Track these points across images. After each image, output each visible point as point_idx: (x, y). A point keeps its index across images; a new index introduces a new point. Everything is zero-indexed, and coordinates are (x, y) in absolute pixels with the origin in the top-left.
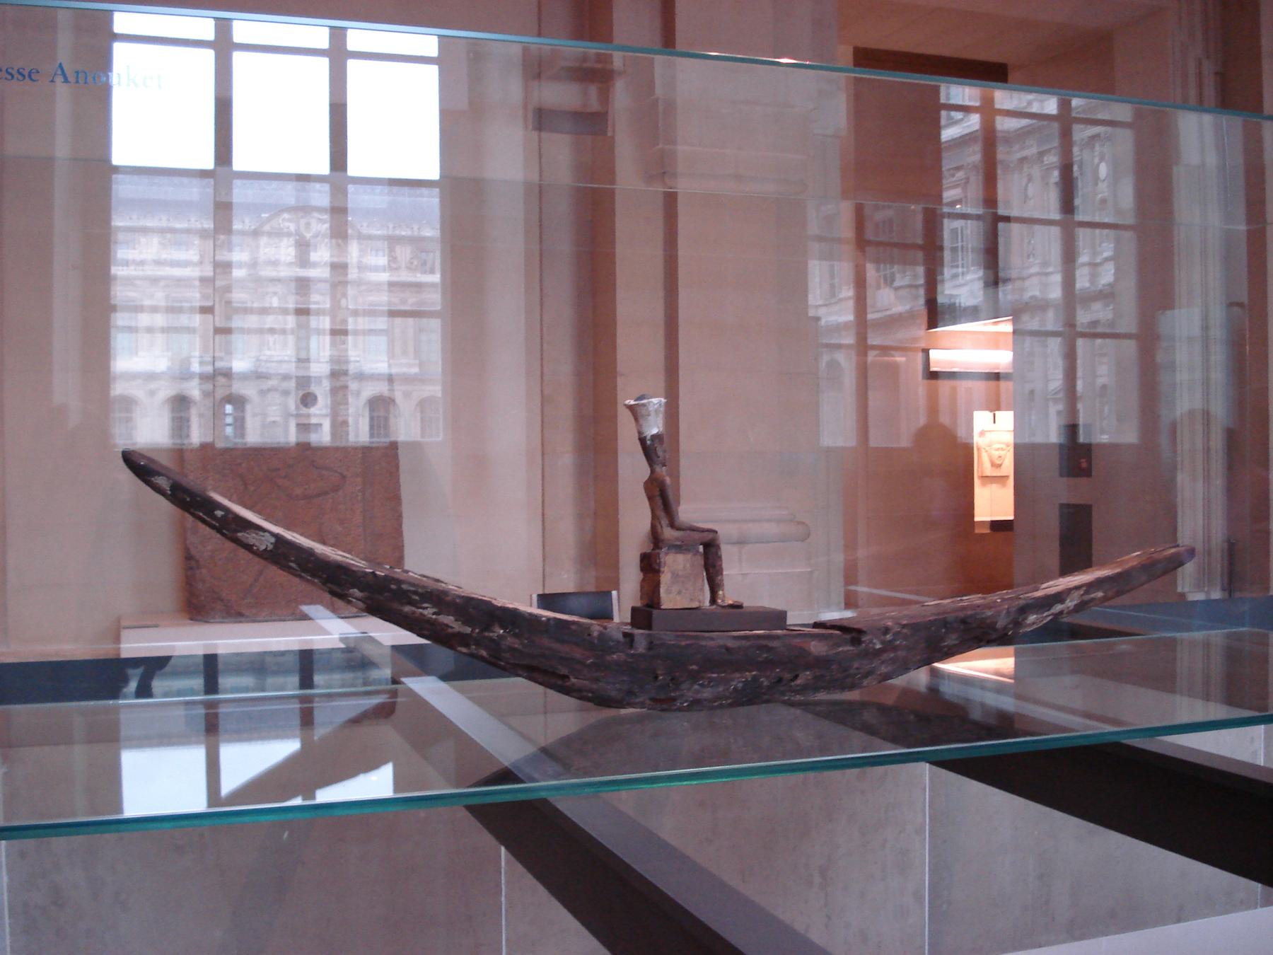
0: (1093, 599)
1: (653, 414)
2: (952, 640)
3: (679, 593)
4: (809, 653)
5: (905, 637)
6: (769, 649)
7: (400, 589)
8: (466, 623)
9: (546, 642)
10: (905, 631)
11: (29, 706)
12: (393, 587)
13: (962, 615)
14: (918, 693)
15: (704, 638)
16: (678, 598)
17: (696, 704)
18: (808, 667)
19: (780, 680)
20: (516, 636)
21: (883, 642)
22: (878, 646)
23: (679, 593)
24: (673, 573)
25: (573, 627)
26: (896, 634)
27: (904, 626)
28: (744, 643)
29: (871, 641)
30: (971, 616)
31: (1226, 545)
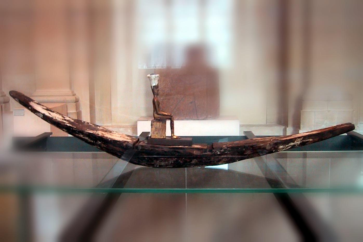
0: (308, 142)
1: (153, 80)
2: (248, 152)
3: (157, 134)
4: (193, 154)
5: (229, 151)
6: (178, 152)
7: (73, 130)
8: (91, 139)
9: (111, 146)
10: (229, 149)
11: (67, 152)
12: (71, 129)
13: (251, 145)
14: (227, 170)
15: (157, 147)
16: (157, 135)
17: (161, 166)
18: (194, 158)
19: (186, 162)
20: (104, 144)
21: (220, 152)
22: (219, 153)
23: (157, 134)
24: (155, 128)
25: (118, 142)
26: (225, 150)
27: (228, 147)
28: (172, 150)
29: (216, 152)
30: (255, 145)
31: (179, 62)
